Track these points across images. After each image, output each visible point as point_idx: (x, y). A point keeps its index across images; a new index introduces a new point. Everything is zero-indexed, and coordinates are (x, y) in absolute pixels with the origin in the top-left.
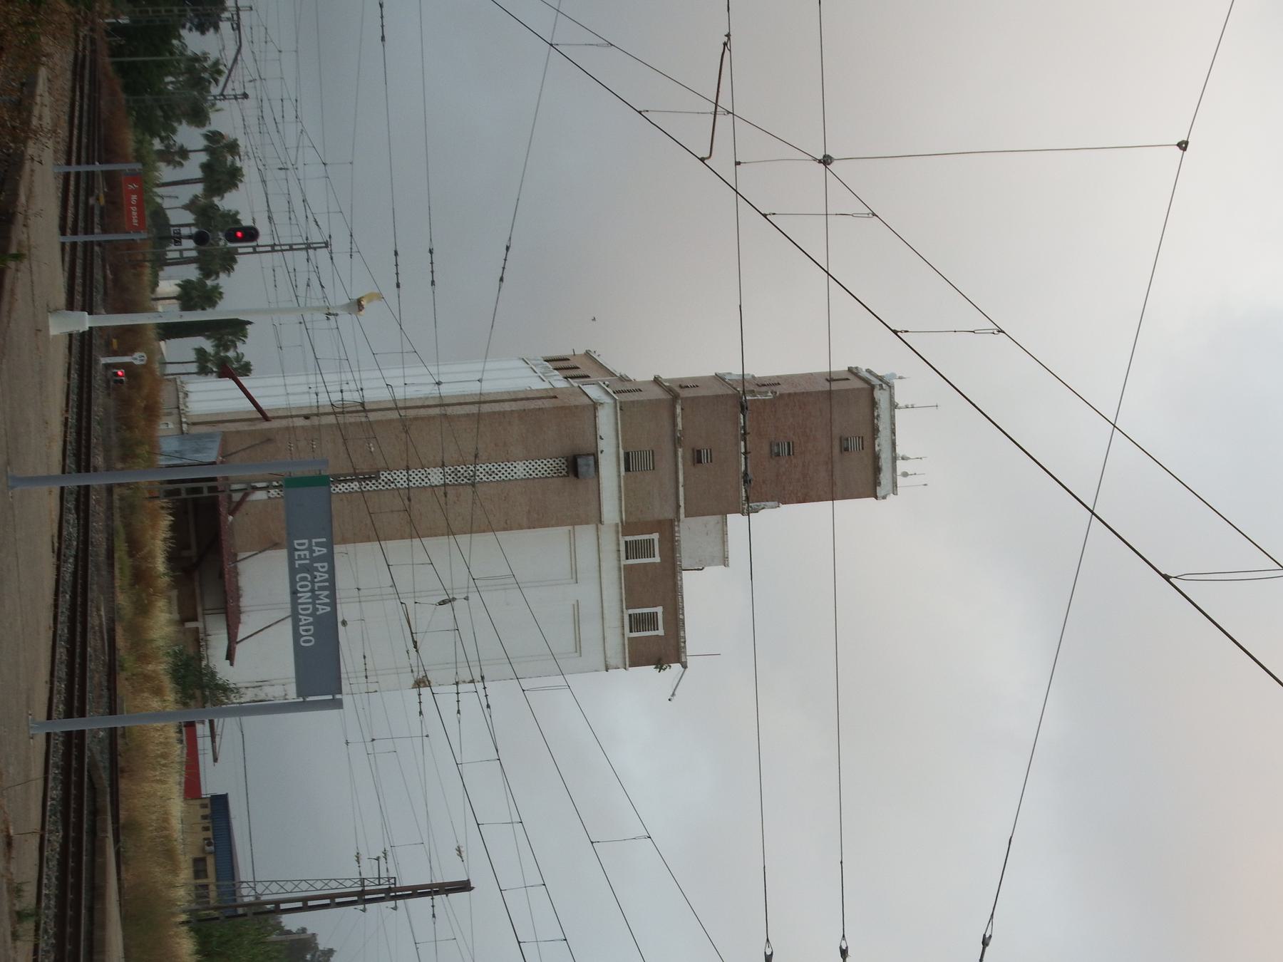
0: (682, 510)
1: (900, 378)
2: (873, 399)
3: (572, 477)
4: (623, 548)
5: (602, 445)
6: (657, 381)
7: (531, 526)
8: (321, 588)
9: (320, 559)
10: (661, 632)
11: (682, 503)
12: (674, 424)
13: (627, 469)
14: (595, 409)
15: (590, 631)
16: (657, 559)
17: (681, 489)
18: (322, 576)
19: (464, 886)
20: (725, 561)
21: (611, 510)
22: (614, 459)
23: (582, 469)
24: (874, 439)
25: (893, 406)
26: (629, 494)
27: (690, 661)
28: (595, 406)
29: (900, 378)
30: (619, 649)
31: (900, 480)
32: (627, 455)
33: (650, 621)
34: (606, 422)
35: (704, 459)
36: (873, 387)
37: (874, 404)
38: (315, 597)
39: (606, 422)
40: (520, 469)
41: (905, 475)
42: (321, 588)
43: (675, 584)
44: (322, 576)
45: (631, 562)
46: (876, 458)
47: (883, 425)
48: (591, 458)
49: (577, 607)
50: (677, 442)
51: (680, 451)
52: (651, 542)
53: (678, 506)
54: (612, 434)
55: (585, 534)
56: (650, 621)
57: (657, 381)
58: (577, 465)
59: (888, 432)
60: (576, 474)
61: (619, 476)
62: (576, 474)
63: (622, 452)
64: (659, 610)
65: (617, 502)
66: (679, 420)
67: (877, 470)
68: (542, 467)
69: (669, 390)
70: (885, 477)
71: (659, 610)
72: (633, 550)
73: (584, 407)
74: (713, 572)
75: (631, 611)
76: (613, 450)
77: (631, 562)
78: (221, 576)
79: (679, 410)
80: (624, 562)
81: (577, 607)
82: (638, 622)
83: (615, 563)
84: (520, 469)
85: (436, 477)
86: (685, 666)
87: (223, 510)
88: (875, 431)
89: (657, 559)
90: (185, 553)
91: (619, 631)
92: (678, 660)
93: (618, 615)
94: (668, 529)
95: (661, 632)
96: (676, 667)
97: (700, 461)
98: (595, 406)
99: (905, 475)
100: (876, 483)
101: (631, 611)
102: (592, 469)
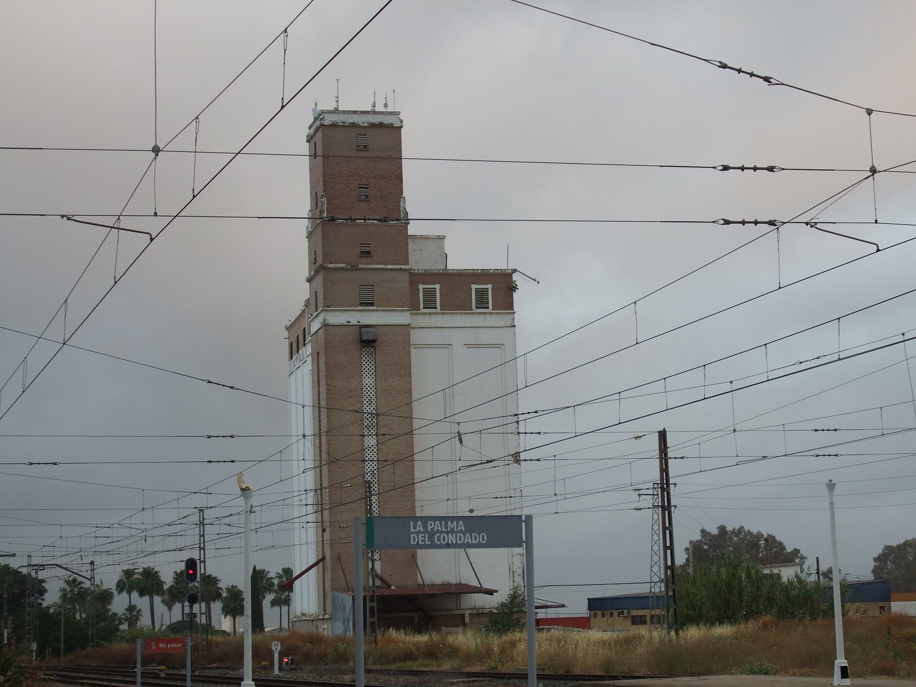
0: (403, 267)
1: (316, 105)
2: (330, 125)
3: (376, 344)
4: (428, 311)
5: (354, 322)
6: (309, 280)
7: (409, 375)
8: (446, 527)
9: (425, 526)
10: (490, 287)
11: (398, 267)
12: (342, 269)
13: (372, 304)
14: (328, 325)
15: (486, 337)
16: (438, 286)
17: (389, 267)
18: (437, 526)
19: (663, 435)
20: (441, 238)
21: (401, 318)
22: (363, 314)
23: (371, 337)
24: (359, 126)
25: (336, 111)
26: (390, 305)
27: (511, 267)
28: (325, 325)
29: (316, 105)
30: (500, 316)
31: (390, 109)
32: (362, 304)
33: (481, 294)
34: (337, 318)
35: (368, 249)
36: (322, 125)
37: (334, 125)
38: (452, 531)
39: (337, 318)
40: (368, 381)
41: (386, 105)
42: (446, 527)
43: (456, 274)
44: (437, 526)
45: (438, 306)
46: (373, 126)
47: (350, 119)
48: (363, 329)
49: (469, 346)
50: (354, 268)
51: (361, 266)
52: (425, 290)
53: (400, 269)
54: (347, 314)
55: (416, 337)
56: (481, 294)
57: (309, 280)
58: (367, 340)
59: (355, 116)
60: (375, 341)
61: (377, 310)
62: (375, 341)
63: (360, 308)
64: (474, 287)
65: (395, 313)
66: (338, 265)
67: (381, 125)
68: (368, 366)
69: (317, 272)
70: (387, 120)
71: (474, 287)
72: (430, 303)
73: (326, 334)
74: (448, 248)
75: (474, 307)
76: (358, 314)
77: (438, 306)
78: (433, 596)
79: (332, 266)
80: (438, 310)
81: (469, 346)
82: (482, 303)
83: (440, 316)
84: (368, 381)
85: (371, 441)
86: (515, 271)
87: (387, 592)
88: (353, 125)
89: (438, 286)
90: (416, 620)
91: (487, 317)
92: (510, 275)
93: (476, 316)
94: (416, 278)
95: (490, 287)
96: (515, 277)
97: (369, 252)
98: (325, 325)
99: (386, 105)
100: (391, 126)
101: (474, 307)
102: (370, 329)
